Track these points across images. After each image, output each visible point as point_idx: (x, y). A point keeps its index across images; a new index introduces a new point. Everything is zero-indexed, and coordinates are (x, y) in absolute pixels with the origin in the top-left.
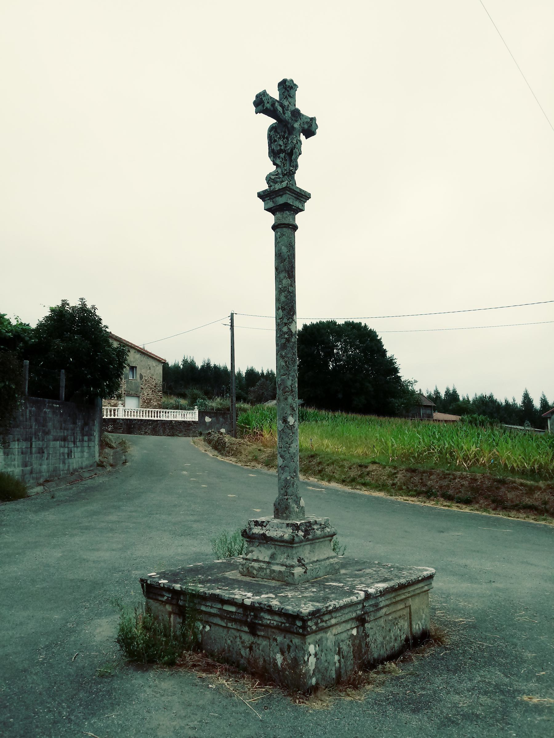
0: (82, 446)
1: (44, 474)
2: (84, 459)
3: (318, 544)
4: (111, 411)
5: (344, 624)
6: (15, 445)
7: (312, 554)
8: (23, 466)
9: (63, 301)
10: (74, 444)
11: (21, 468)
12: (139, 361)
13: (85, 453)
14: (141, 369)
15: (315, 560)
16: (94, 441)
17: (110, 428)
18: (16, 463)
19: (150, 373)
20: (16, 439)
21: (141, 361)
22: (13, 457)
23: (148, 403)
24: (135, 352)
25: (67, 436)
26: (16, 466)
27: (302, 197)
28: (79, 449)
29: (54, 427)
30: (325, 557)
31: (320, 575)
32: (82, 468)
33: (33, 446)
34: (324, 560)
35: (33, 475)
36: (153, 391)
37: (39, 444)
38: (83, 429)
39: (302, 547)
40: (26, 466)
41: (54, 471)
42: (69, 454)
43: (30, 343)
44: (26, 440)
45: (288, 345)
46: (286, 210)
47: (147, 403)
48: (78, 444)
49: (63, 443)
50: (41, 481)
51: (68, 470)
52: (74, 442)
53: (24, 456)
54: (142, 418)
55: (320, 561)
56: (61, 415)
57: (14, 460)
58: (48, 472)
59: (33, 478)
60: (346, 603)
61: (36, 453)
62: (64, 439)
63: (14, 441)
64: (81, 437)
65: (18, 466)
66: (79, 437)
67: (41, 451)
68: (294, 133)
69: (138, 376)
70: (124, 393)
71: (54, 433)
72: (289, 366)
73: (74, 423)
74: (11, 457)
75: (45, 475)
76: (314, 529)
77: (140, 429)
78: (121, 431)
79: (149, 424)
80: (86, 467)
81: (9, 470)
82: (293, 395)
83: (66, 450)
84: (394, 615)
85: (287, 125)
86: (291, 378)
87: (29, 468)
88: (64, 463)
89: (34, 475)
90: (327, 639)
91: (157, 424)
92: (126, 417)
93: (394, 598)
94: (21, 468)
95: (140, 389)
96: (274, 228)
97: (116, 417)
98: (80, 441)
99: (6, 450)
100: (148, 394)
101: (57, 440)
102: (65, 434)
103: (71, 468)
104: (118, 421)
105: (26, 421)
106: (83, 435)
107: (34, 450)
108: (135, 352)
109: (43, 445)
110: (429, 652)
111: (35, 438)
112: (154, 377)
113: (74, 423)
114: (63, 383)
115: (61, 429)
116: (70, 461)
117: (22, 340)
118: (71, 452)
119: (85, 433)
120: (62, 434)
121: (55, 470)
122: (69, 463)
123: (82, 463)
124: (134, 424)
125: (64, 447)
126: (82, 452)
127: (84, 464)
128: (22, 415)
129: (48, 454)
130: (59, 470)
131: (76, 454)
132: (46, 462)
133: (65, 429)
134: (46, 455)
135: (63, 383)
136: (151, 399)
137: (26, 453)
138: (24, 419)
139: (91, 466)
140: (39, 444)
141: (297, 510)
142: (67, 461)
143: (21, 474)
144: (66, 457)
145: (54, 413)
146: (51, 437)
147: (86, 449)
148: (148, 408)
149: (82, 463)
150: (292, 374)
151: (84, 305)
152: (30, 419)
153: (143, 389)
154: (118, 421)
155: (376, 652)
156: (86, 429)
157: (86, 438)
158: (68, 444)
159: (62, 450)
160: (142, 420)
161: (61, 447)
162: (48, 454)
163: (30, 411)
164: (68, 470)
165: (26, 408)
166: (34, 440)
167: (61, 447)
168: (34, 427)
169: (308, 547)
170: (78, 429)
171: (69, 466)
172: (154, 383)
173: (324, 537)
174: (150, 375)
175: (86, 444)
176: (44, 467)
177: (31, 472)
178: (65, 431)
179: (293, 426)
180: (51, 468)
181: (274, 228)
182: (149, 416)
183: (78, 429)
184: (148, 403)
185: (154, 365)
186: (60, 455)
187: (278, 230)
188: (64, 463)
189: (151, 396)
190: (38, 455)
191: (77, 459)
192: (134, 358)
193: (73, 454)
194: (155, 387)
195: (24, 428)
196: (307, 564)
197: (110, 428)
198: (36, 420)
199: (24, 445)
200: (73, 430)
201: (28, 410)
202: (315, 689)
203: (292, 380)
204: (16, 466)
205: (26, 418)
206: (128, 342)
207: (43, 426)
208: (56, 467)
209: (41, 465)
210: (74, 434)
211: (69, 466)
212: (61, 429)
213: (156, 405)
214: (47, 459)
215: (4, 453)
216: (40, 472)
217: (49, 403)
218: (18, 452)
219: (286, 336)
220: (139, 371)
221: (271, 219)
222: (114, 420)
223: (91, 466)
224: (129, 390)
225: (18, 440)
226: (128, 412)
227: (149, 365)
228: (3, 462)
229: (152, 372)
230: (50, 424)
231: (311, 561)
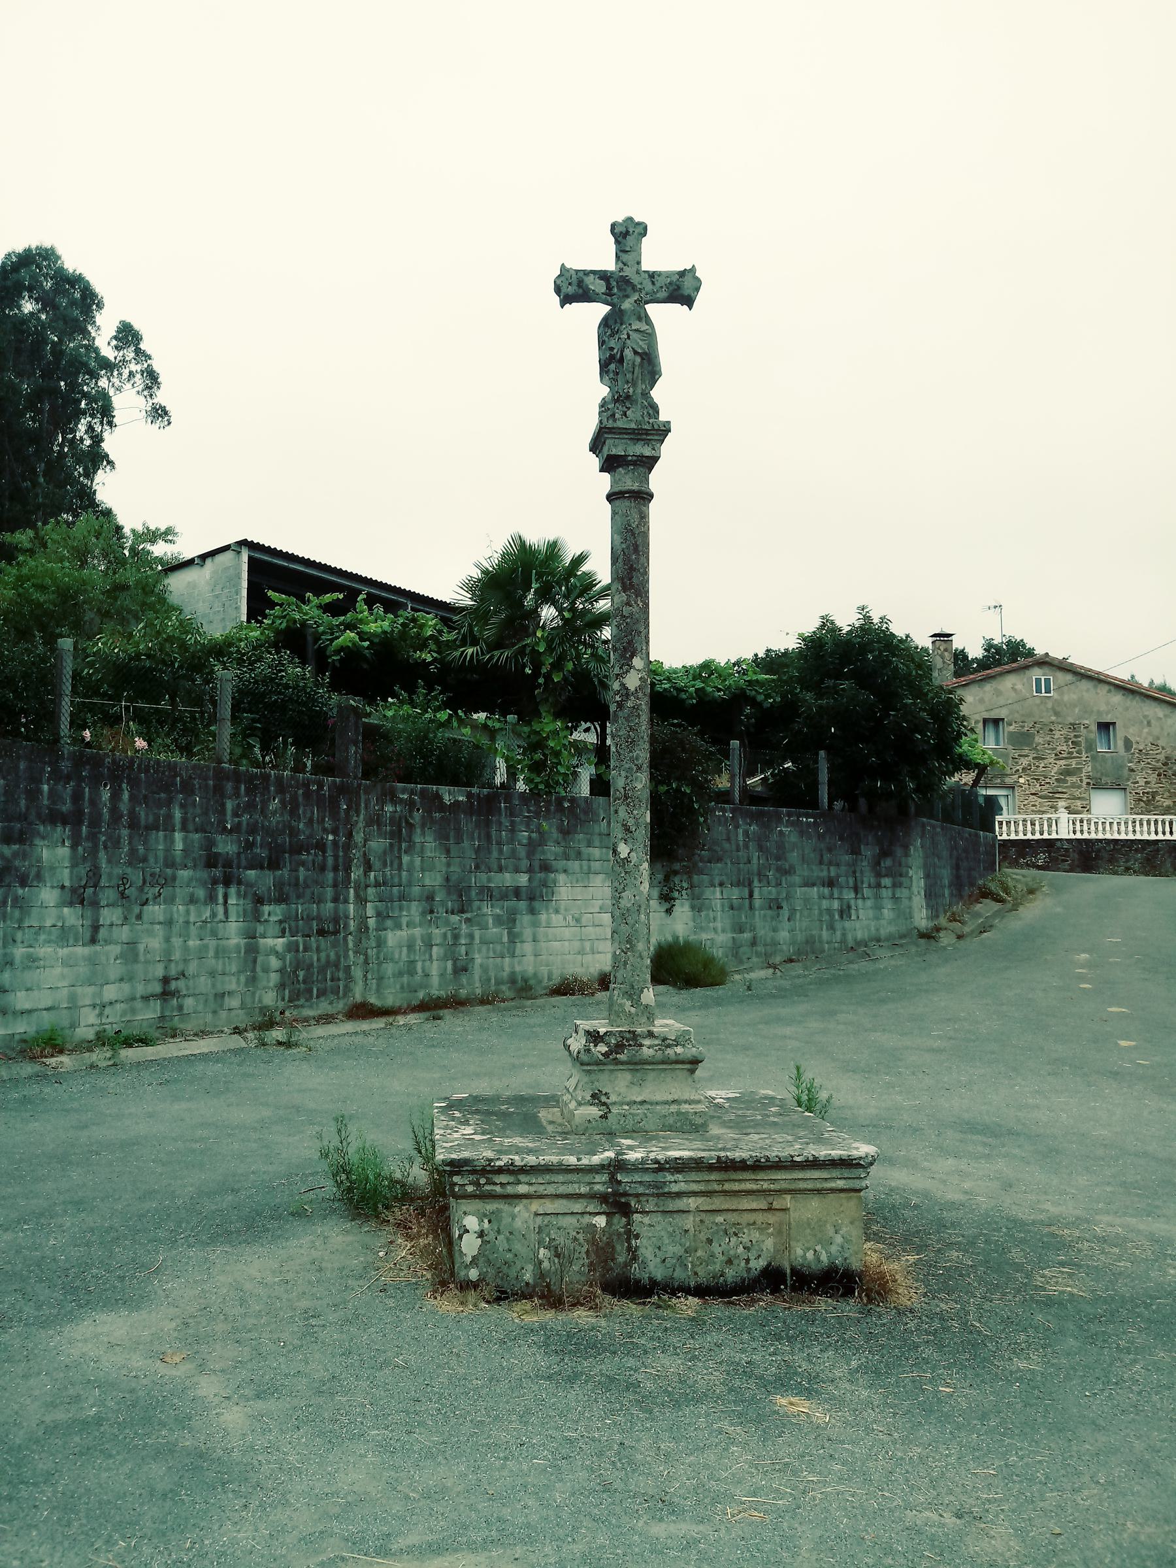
0: (878, 897)
1: (784, 947)
2: (884, 922)
3: (651, 1075)
4: (1033, 824)
5: (564, 1202)
6: (714, 893)
7: (636, 1089)
8: (734, 931)
9: (822, 617)
10: (856, 892)
11: (730, 935)
12: (1120, 709)
13: (885, 911)
14: (1126, 727)
15: (639, 1099)
16: (910, 888)
17: (1041, 859)
18: (719, 925)
19: (1149, 733)
20: (717, 882)
21: (1127, 709)
22: (711, 914)
23: (1148, 803)
24: (1109, 691)
25: (838, 876)
26: (720, 930)
27: (647, 434)
28: (869, 903)
29: (803, 859)
30: (670, 1098)
31: (647, 1128)
32: (878, 940)
33: (756, 894)
34: (666, 1103)
35: (759, 949)
36: (1159, 775)
37: (770, 893)
38: (879, 863)
39: (606, 1073)
40: (741, 931)
41: (807, 942)
42: (845, 912)
43: (766, 705)
44: (738, 884)
45: (620, 714)
46: (618, 467)
47: (1145, 803)
48: (867, 892)
49: (826, 891)
50: (778, 959)
51: (843, 941)
52: (856, 889)
53: (736, 912)
54: (1116, 836)
55: (651, 1104)
56: (820, 837)
57: (714, 919)
58: (793, 943)
59: (758, 955)
60: (543, 1163)
61: (762, 909)
62: (831, 883)
63: (713, 885)
64: (872, 880)
65: (723, 931)
66: (868, 878)
67: (775, 906)
68: (625, 319)
69: (1120, 743)
70: (1088, 784)
71: (802, 871)
72: (621, 752)
73: (855, 851)
74: (708, 915)
75: (788, 950)
76: (641, 1045)
77: (1112, 860)
78: (1066, 865)
79: (1137, 850)
80: (890, 937)
81: (704, 936)
82: (628, 805)
83: (836, 905)
84: (733, 1218)
85: (625, 298)
86: (623, 774)
87: (747, 936)
88: (831, 928)
89: (760, 949)
90: (513, 1217)
91: (1158, 850)
92: (1079, 836)
93: (719, 1182)
94: (730, 935)
95: (1126, 772)
96: (610, 497)
97: (1054, 836)
98: (870, 886)
99: (696, 902)
100: (1147, 783)
101: (813, 885)
102: (833, 874)
103: (850, 937)
104: (1058, 844)
105: (738, 850)
106: (879, 875)
107: (757, 903)
108: (1109, 691)
109: (778, 893)
110: (850, 1308)
111: (760, 881)
112: (1161, 743)
113: (855, 851)
114: (824, 776)
115: (821, 863)
116: (847, 924)
117: (753, 702)
118: (849, 907)
119: (884, 871)
120: (825, 873)
121: (810, 941)
122: (844, 929)
123: (877, 930)
124: (1099, 851)
125: (831, 897)
126: (878, 908)
127: (883, 933)
128: (728, 840)
129: (793, 911)
130: (821, 942)
131: (861, 911)
132: (787, 925)
133: (830, 863)
134: (785, 913)
135: (824, 776)
136: (1154, 794)
137: (740, 908)
138: (734, 847)
139: (902, 936)
140: (770, 893)
141: (633, 1010)
142: (838, 925)
143: (730, 944)
144: (837, 917)
145: (802, 833)
146: (797, 879)
147: (888, 904)
148: (1149, 812)
149: (877, 930)
150: (627, 766)
151: (867, 618)
152: (746, 846)
153: (1133, 770)
154: (1058, 844)
155: (652, 1266)
156: (888, 862)
157: (887, 881)
158: (841, 893)
159: (825, 904)
160: (1116, 841)
161: (822, 897)
162: (793, 911)
163: (746, 833)
164: (843, 941)
165: (737, 827)
166: (756, 883)
167: (822, 897)
168: (755, 861)
169: (628, 1076)
170: (865, 863)
171: (844, 935)
172: (1162, 757)
173: (663, 1062)
174: (1150, 739)
175: (885, 893)
176: (783, 935)
177: (754, 943)
178: (832, 868)
179: (627, 860)
180: (800, 937)
181: (610, 497)
182: (1156, 833)
183: (865, 863)
184: (1148, 803)
185: (1161, 714)
186: (821, 914)
187: (617, 503)
188: (831, 928)
189: (1154, 787)
190: (769, 912)
191: (866, 922)
192: (1107, 703)
193: (853, 912)
194: (1165, 764)
195: (732, 863)
196: (614, 1103)
197: (1041, 859)
198: (761, 848)
199: (735, 893)
200: (854, 864)
201: (740, 831)
202: (466, 1286)
203: (627, 777)
204: (720, 930)
205: (738, 845)
206: (1090, 670)
207: (778, 858)
208: (812, 936)
209: (775, 930)
210: (854, 872)
211: (844, 935)
212: (821, 863)
213: (1169, 807)
214: (789, 920)
215: (693, 907)
216: (775, 943)
217: (789, 815)
218: (723, 906)
219: (618, 698)
220: (1120, 733)
221: (604, 482)
222: (1050, 843)
223: (902, 936)
224: (1099, 775)
225: (721, 885)
226: (1111, 823)
227: (1145, 717)
228: (691, 924)
229: (1156, 731)
230: (794, 857)
231: (628, 1099)
